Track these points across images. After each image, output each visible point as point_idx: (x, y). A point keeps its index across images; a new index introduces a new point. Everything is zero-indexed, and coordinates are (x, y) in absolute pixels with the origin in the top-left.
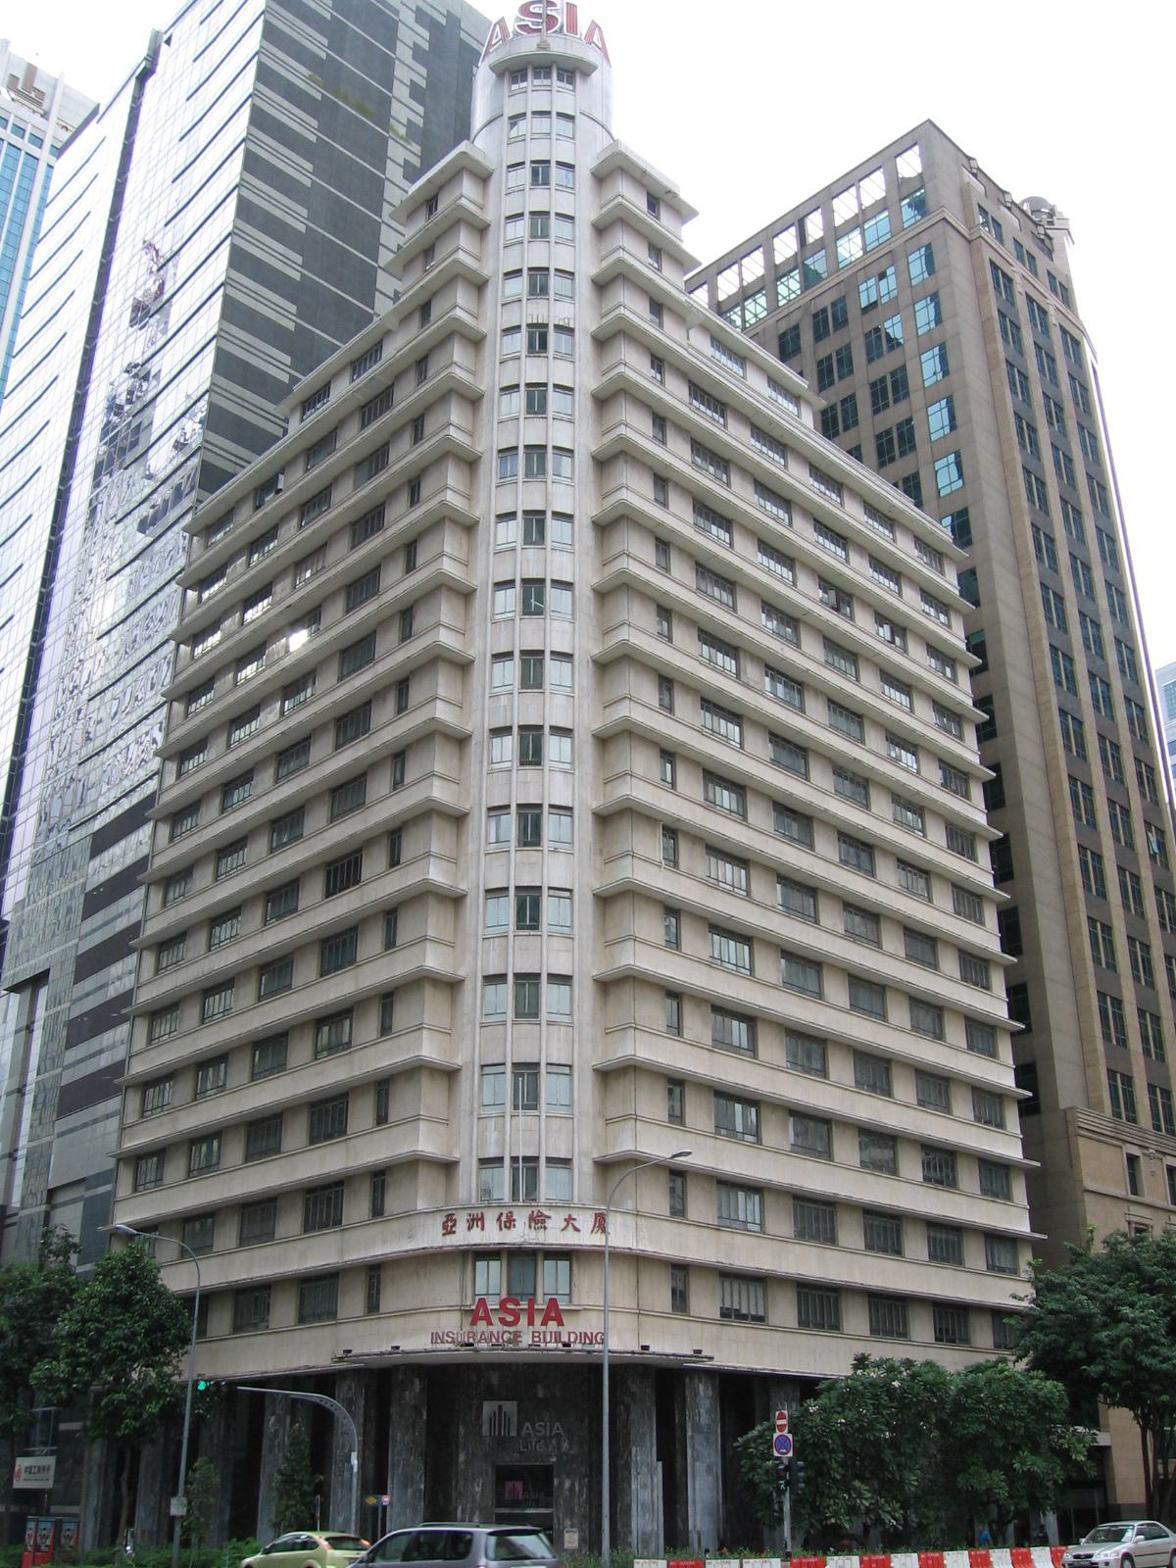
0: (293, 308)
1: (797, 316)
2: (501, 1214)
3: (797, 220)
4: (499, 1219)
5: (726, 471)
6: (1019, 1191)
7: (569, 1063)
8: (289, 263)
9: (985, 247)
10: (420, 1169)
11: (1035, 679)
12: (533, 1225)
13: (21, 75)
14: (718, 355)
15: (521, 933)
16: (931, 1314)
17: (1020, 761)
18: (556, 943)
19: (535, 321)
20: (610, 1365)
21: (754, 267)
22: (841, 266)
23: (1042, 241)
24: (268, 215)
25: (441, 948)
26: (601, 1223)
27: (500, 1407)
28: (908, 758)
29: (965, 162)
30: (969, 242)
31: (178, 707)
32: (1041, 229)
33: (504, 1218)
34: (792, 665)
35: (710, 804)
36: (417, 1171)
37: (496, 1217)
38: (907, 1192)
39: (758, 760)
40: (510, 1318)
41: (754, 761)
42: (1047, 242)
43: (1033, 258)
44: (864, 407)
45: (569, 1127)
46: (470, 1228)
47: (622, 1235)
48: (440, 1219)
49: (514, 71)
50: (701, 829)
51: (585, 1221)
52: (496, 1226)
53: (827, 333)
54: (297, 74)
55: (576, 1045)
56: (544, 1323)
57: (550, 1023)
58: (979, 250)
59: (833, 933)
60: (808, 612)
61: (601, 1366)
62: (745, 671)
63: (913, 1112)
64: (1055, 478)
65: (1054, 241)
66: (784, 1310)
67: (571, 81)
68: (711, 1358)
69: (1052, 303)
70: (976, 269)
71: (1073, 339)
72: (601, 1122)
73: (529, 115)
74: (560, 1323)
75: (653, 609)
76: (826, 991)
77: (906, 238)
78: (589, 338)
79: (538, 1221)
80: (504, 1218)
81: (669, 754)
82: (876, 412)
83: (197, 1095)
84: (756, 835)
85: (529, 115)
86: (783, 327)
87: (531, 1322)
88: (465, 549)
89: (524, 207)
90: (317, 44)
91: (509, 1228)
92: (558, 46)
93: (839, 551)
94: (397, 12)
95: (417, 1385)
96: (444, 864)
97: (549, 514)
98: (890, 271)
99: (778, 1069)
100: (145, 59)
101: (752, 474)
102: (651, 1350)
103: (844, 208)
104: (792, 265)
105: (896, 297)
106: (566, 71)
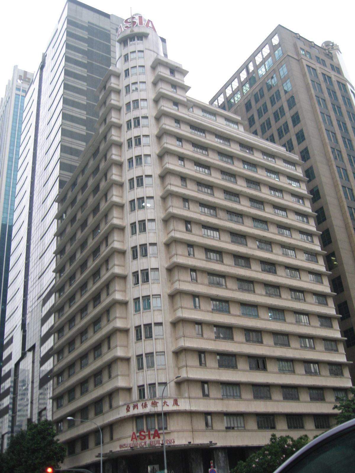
0: (85, 128)
1: (249, 97)
2: (143, 403)
3: (245, 66)
4: (142, 405)
5: (252, 150)
6: (347, 373)
7: (164, 351)
8: (82, 115)
9: (303, 61)
10: (120, 392)
11: (339, 199)
12: (153, 406)
13: (22, 75)
14: (205, 114)
15: (145, 311)
16: (286, 420)
17: (335, 227)
18: (156, 313)
19: (135, 117)
20: (166, 452)
21: (235, 84)
22: (260, 77)
23: (328, 55)
24: (73, 101)
25: (121, 320)
26: (176, 403)
27: (154, 467)
28: (287, 232)
29: (295, 35)
30: (298, 60)
31: (58, 256)
32: (328, 51)
33: (144, 405)
34: (236, 209)
35: (208, 259)
36: (119, 392)
37: (141, 404)
38: (299, 378)
39: (226, 242)
40: (143, 438)
41: (226, 244)
42: (330, 54)
43: (324, 61)
44: (273, 121)
45: (164, 371)
46: (134, 409)
47: (184, 405)
48: (125, 407)
49: (124, 41)
50: (204, 268)
51: (170, 402)
52: (141, 407)
53: (259, 100)
54: (79, 57)
55: (165, 345)
56: (154, 438)
57: (156, 339)
58: (302, 62)
59: (261, 295)
60: (241, 191)
61: (163, 452)
62: (219, 214)
63: (298, 351)
64: (339, 131)
65: (333, 54)
66: (252, 424)
67: (142, 40)
68: (216, 444)
69: (333, 75)
70: (302, 69)
71: (342, 84)
72: (176, 369)
73: (137, 52)
74: (159, 437)
75: (181, 200)
76: (260, 314)
77: (277, 65)
78: (154, 118)
79: (154, 404)
80: (144, 405)
81: (190, 245)
82: (276, 122)
83: (69, 376)
84: (228, 267)
85: (137, 52)
86: (246, 101)
87: (150, 438)
88: (121, 192)
89: (130, 82)
90: (84, 46)
91: (146, 407)
92: (136, 30)
93: (293, 167)
94: (110, 31)
95: (124, 463)
96: (121, 293)
97: (144, 176)
98: (274, 76)
99: (242, 343)
100: (41, 62)
101: (216, 150)
102: (213, 442)
103: (259, 59)
104: (246, 81)
105: (277, 84)
106: (140, 37)
